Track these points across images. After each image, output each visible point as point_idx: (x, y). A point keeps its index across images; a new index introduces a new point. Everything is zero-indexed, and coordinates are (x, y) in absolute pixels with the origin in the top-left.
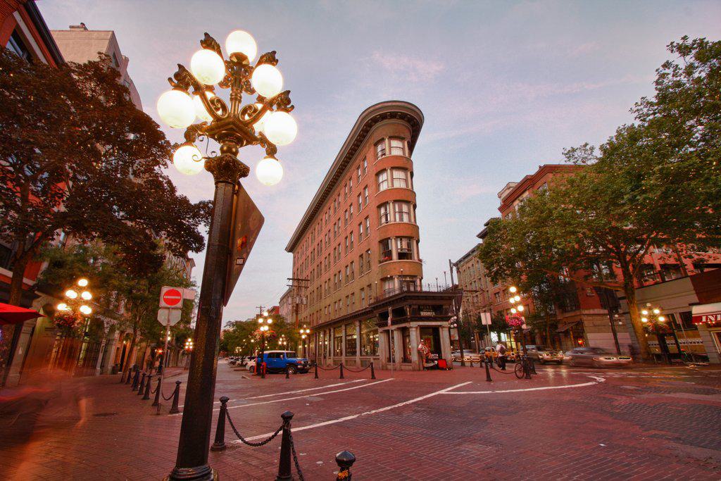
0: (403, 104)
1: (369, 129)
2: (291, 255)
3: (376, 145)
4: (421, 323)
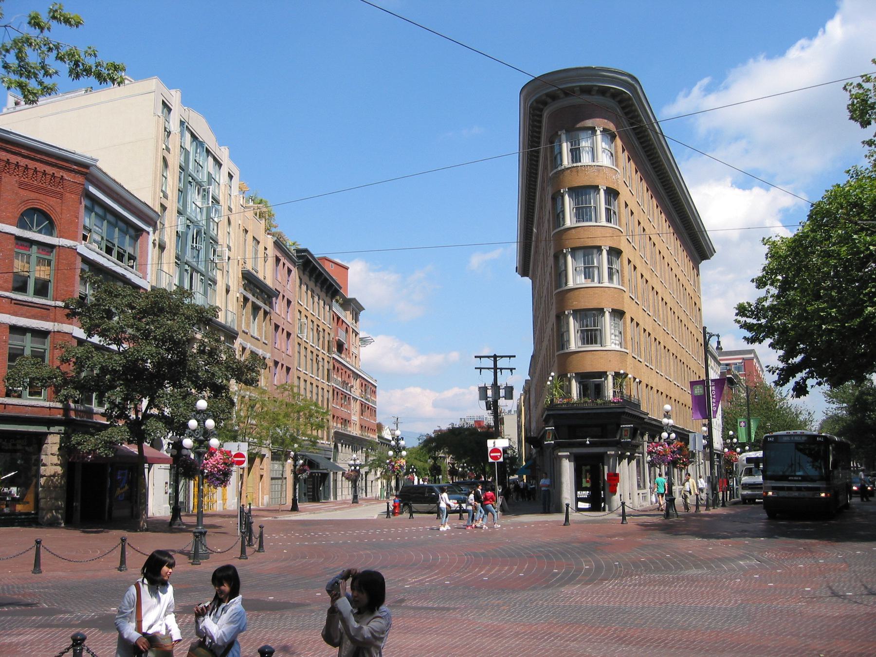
1: (562, 95)
2: (527, 281)
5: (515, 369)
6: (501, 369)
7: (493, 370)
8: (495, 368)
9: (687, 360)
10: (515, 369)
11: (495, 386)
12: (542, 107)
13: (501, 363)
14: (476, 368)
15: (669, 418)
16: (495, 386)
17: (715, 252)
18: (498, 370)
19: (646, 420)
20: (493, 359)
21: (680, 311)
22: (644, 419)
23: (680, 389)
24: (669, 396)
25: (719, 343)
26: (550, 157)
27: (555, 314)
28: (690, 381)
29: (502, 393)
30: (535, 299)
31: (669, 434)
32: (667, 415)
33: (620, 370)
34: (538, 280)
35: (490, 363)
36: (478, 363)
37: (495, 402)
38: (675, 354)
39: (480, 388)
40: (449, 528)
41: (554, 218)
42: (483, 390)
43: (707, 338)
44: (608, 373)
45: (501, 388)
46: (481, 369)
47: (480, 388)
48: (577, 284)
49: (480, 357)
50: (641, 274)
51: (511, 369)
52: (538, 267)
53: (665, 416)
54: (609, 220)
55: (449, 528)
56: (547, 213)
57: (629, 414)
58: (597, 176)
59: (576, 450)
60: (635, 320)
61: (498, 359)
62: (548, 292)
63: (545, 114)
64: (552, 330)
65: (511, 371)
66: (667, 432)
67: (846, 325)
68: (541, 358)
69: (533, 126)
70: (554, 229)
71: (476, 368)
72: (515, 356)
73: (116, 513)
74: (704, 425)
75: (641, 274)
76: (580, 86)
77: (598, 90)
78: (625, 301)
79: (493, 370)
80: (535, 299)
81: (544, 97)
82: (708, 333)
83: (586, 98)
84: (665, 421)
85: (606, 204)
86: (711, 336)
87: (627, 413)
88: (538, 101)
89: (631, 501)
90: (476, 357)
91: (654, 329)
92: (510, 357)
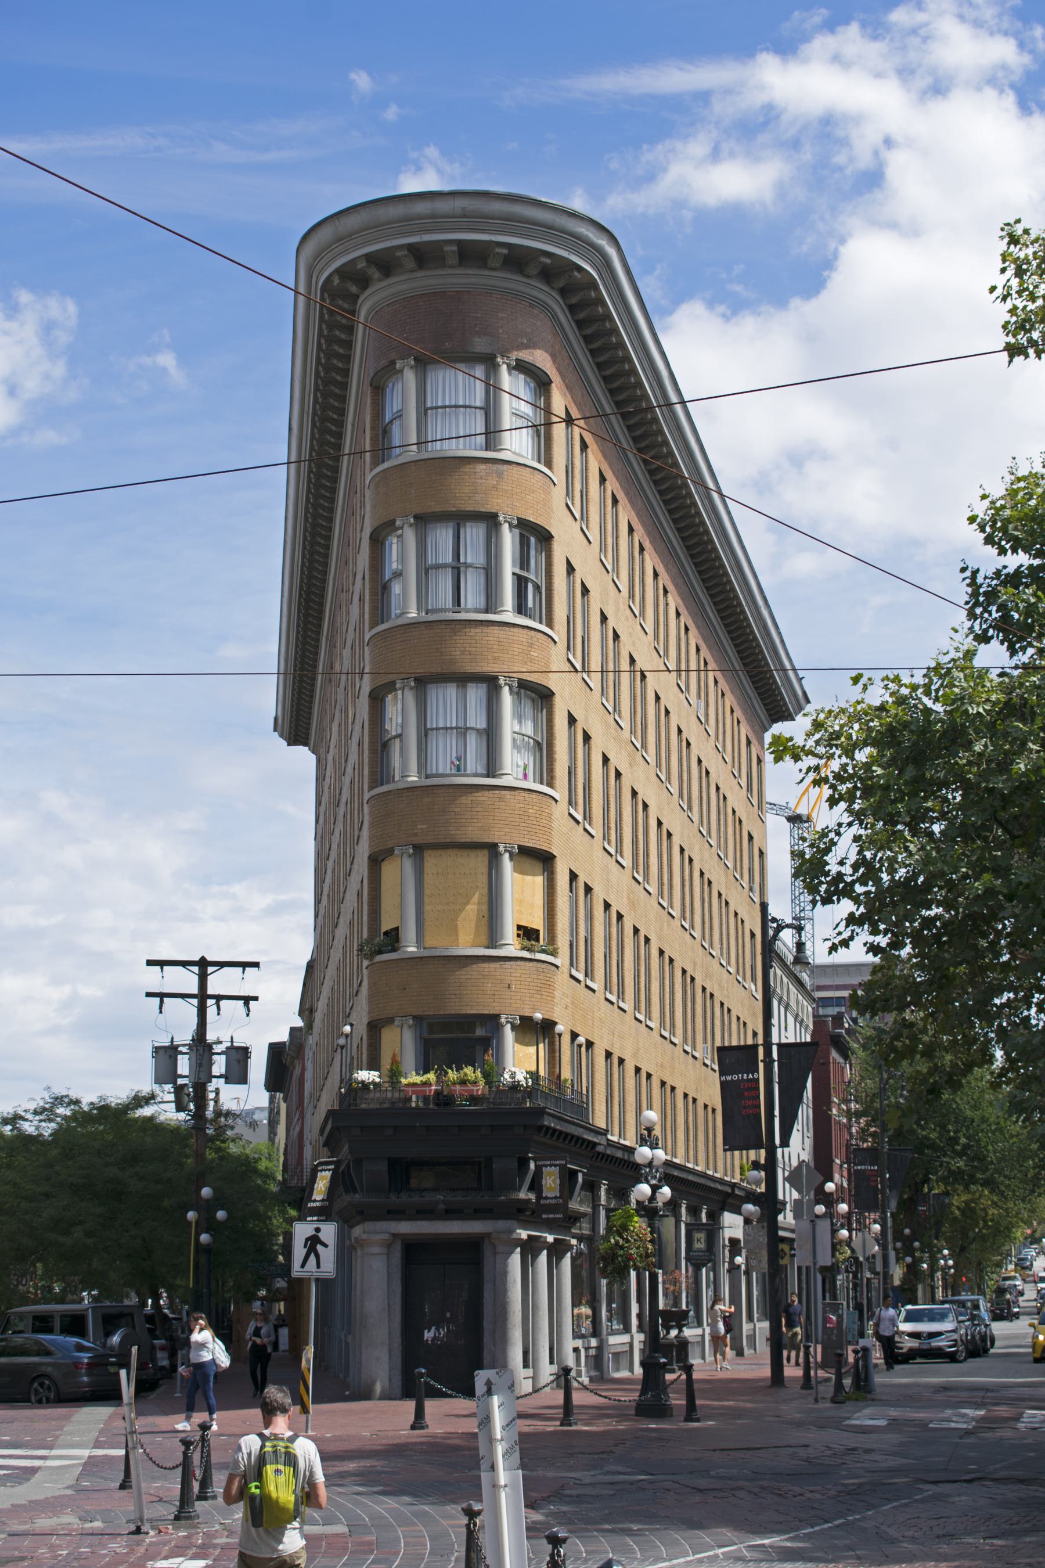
0: (459, 203)
1: (453, 260)
2: (304, 758)
3: (378, 389)
4: (406, 1227)
5: (256, 999)
6: (219, 998)
7: (195, 1001)
8: (202, 996)
9: (721, 987)
10: (256, 999)
11: (201, 1046)
12: (354, 289)
13: (218, 982)
14: (149, 995)
15: (654, 1146)
16: (201, 1046)
17: (808, 701)
18: (210, 1002)
19: (600, 1149)
20: (196, 969)
21: (706, 855)
22: (595, 1144)
23: (699, 1064)
24: (670, 1082)
25: (800, 946)
26: (372, 428)
27: (366, 855)
28: (718, 1043)
29: (219, 1065)
30: (322, 809)
31: (655, 1189)
32: (647, 1138)
33: (535, 1010)
34: (330, 757)
35: (188, 982)
36: (154, 980)
37: (200, 1088)
38: (690, 972)
39: (157, 1050)
40: (865, 911)
41: (373, 593)
42: (166, 1055)
43: (771, 932)
44: (503, 1020)
45: (218, 1048)
46: (162, 996)
47: (157, 1050)
48: (427, 777)
49: (162, 964)
50: (604, 755)
51: (247, 1000)
52: (332, 720)
53: (643, 1141)
54: (521, 608)
55: (865, 911)
56: (359, 577)
57: (555, 1130)
58: (494, 486)
59: (406, 1227)
60: (582, 879)
61: (210, 969)
62: (352, 795)
63: (365, 308)
64: (359, 894)
65: (247, 1004)
66: (648, 1182)
67: (428, 1335)
68: (331, 972)
69: (331, 340)
70: (373, 625)
71: (149, 995)
72: (256, 965)
73: (455, 248)
74: (756, 1165)
75: (604, 755)
76: (337, 271)
77: (506, 257)
78: (555, 825)
79: (195, 1001)
80: (322, 809)
81: (362, 265)
82: (774, 920)
83: (471, 277)
84: (644, 1153)
85: (514, 565)
86: (780, 928)
87: (548, 1128)
88: (344, 273)
89: (530, 1372)
90: (150, 963)
91: (633, 904)
92: (244, 965)
